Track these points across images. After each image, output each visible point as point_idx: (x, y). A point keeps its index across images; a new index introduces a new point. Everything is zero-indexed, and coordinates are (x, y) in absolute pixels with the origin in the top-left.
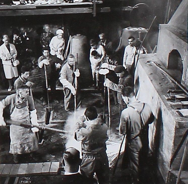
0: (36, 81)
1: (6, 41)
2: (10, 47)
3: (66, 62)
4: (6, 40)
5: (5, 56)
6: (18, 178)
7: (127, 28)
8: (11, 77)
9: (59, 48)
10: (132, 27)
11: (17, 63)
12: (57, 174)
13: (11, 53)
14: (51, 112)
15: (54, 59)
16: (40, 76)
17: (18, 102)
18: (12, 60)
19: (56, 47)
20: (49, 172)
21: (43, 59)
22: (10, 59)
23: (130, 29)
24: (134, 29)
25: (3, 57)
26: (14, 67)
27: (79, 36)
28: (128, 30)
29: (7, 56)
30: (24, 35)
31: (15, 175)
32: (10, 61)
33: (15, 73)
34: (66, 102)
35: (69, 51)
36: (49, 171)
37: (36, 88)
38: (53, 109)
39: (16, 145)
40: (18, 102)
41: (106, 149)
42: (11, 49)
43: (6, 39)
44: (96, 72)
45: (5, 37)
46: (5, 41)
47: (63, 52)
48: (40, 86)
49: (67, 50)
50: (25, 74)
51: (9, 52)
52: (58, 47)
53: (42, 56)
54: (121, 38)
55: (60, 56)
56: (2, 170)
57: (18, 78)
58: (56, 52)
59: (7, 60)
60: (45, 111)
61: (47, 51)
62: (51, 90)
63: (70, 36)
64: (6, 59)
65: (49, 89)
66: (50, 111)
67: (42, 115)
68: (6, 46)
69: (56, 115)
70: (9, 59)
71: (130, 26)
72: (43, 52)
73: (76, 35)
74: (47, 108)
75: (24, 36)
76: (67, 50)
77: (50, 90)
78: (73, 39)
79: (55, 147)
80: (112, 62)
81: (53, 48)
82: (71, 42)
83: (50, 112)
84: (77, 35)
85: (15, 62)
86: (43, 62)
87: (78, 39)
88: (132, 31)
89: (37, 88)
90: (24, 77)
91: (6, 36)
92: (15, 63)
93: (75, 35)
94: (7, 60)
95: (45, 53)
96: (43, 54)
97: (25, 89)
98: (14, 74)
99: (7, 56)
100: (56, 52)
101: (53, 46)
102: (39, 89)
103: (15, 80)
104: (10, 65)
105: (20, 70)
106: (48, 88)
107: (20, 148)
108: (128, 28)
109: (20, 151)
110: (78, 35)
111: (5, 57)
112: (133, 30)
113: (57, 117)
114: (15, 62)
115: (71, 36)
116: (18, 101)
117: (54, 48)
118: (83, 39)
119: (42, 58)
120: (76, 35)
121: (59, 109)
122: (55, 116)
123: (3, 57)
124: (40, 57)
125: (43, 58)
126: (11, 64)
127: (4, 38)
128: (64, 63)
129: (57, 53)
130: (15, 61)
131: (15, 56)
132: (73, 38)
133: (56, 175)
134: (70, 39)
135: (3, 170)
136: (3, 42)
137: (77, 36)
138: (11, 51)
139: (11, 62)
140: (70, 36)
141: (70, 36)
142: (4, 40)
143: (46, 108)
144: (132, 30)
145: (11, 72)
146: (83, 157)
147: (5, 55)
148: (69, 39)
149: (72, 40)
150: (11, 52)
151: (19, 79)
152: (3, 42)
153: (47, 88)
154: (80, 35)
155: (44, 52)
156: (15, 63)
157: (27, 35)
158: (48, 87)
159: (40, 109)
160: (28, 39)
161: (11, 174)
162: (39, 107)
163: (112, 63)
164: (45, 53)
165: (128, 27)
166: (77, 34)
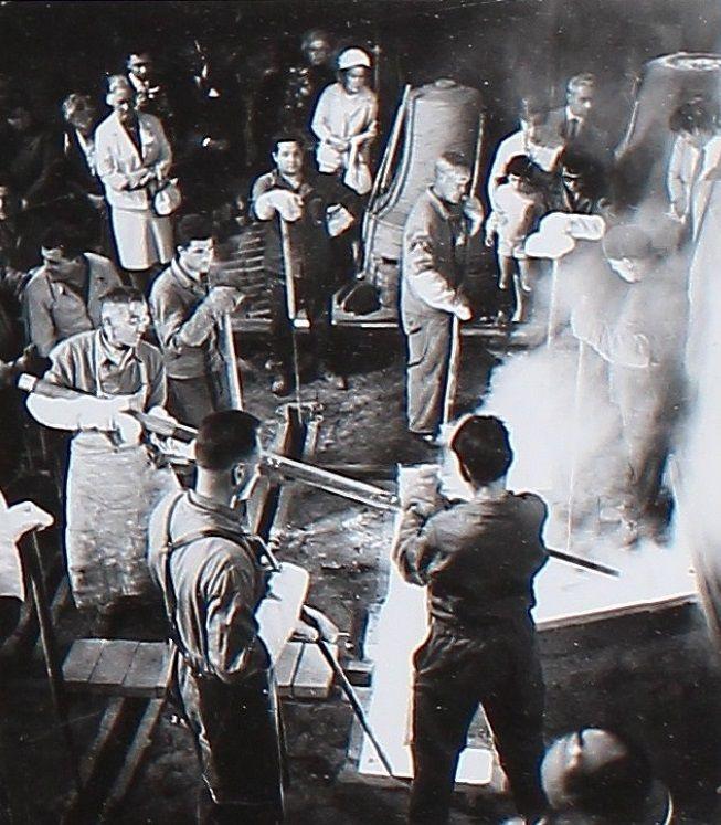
0: (247, 283)
1: (122, 102)
2: (142, 132)
3: (382, 204)
4: (121, 98)
5: (120, 171)
6: (160, 701)
7: (669, 57)
8: (145, 259)
9: (356, 134)
10: (692, 52)
11: (171, 200)
12: (325, 693)
13: (144, 156)
14: (309, 427)
15: (324, 188)
16: (259, 263)
17: (108, 363)
18: (153, 188)
19: (342, 134)
20: (292, 685)
21: (276, 187)
22: (143, 182)
23: (682, 62)
24: (699, 62)
25: (111, 173)
26: (162, 219)
27: (446, 88)
28: (672, 66)
29: (128, 168)
30: (200, 75)
31: (149, 689)
32: (144, 192)
33: (164, 246)
34: (416, 394)
35: (401, 156)
36: (293, 680)
37: (248, 317)
38: (319, 413)
39: (113, 561)
40: (108, 363)
41: (534, 603)
42: (146, 138)
43: (120, 95)
44: (516, 256)
45: (115, 88)
46: (116, 105)
47: (373, 154)
48: (265, 307)
49: (390, 152)
50: (190, 250)
51: (136, 153)
52: (351, 132)
53: (270, 175)
54: (637, 103)
55: (358, 179)
56: (94, 664)
57: (168, 271)
58: (345, 155)
59: (127, 188)
60: (285, 422)
61: (291, 144)
62: (310, 328)
63: (408, 87)
64: (124, 183)
65: (298, 323)
66: (307, 419)
67: (270, 436)
68: (123, 123)
69: (331, 438)
70: (136, 185)
71: (681, 51)
72: (276, 150)
73: (434, 86)
74: (293, 405)
75: (198, 79)
76: (390, 152)
77: (304, 328)
78: (419, 101)
79: (321, 578)
80: (587, 203)
81: (333, 139)
82: (410, 114)
83: (306, 428)
84: (438, 84)
85: (162, 197)
86: (275, 202)
87: (442, 103)
88: (691, 71)
89: (251, 314)
90: (190, 263)
91: (122, 81)
92: (162, 199)
93: (426, 83)
94: (127, 188)
95: (286, 155)
96: (276, 165)
97: (122, 305)
98: (157, 252)
99: (128, 168)
100: (342, 152)
101: (329, 128)
102: (259, 321)
103: (155, 280)
104: (144, 211)
105: (182, 229)
106: (296, 318)
107: (132, 573)
108: (673, 56)
109: (133, 583)
110: (444, 86)
111: (121, 175)
112: (694, 65)
113: (334, 447)
114: (162, 197)
115: (412, 89)
116: (104, 359)
117: (336, 136)
118: (465, 102)
119: (269, 180)
120: (434, 86)
121: (345, 414)
122: (327, 445)
123: (111, 173)
124: (263, 178)
125: (273, 183)
126: (145, 205)
127: (111, 88)
128: (375, 209)
129: (349, 156)
130: (164, 193)
131: (162, 170)
132: (418, 97)
133: (317, 700)
134: (408, 99)
135: (97, 664)
136: (111, 109)
137: (439, 89)
138: (144, 148)
139: (145, 196)
140: (408, 87)
141: (404, 88)
142: (111, 99)
143: (290, 409)
144: (691, 67)
145: (148, 243)
146: (434, 636)
147: (119, 165)
148: (400, 103)
149: (414, 108)
150: (147, 152)
151: (174, 274)
152: (111, 109)
153: (291, 316)
154: (452, 82)
155: (280, 152)
156: (162, 199)
157: (208, 74)
158: (297, 310)
159: (262, 407)
160: (213, 93)
161: (128, 683)
162: (257, 401)
163: (589, 208)
164: (286, 154)
165: (675, 53)
166: (438, 79)
